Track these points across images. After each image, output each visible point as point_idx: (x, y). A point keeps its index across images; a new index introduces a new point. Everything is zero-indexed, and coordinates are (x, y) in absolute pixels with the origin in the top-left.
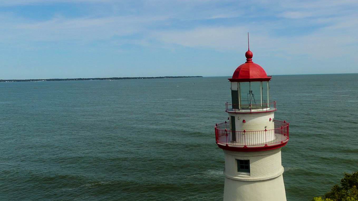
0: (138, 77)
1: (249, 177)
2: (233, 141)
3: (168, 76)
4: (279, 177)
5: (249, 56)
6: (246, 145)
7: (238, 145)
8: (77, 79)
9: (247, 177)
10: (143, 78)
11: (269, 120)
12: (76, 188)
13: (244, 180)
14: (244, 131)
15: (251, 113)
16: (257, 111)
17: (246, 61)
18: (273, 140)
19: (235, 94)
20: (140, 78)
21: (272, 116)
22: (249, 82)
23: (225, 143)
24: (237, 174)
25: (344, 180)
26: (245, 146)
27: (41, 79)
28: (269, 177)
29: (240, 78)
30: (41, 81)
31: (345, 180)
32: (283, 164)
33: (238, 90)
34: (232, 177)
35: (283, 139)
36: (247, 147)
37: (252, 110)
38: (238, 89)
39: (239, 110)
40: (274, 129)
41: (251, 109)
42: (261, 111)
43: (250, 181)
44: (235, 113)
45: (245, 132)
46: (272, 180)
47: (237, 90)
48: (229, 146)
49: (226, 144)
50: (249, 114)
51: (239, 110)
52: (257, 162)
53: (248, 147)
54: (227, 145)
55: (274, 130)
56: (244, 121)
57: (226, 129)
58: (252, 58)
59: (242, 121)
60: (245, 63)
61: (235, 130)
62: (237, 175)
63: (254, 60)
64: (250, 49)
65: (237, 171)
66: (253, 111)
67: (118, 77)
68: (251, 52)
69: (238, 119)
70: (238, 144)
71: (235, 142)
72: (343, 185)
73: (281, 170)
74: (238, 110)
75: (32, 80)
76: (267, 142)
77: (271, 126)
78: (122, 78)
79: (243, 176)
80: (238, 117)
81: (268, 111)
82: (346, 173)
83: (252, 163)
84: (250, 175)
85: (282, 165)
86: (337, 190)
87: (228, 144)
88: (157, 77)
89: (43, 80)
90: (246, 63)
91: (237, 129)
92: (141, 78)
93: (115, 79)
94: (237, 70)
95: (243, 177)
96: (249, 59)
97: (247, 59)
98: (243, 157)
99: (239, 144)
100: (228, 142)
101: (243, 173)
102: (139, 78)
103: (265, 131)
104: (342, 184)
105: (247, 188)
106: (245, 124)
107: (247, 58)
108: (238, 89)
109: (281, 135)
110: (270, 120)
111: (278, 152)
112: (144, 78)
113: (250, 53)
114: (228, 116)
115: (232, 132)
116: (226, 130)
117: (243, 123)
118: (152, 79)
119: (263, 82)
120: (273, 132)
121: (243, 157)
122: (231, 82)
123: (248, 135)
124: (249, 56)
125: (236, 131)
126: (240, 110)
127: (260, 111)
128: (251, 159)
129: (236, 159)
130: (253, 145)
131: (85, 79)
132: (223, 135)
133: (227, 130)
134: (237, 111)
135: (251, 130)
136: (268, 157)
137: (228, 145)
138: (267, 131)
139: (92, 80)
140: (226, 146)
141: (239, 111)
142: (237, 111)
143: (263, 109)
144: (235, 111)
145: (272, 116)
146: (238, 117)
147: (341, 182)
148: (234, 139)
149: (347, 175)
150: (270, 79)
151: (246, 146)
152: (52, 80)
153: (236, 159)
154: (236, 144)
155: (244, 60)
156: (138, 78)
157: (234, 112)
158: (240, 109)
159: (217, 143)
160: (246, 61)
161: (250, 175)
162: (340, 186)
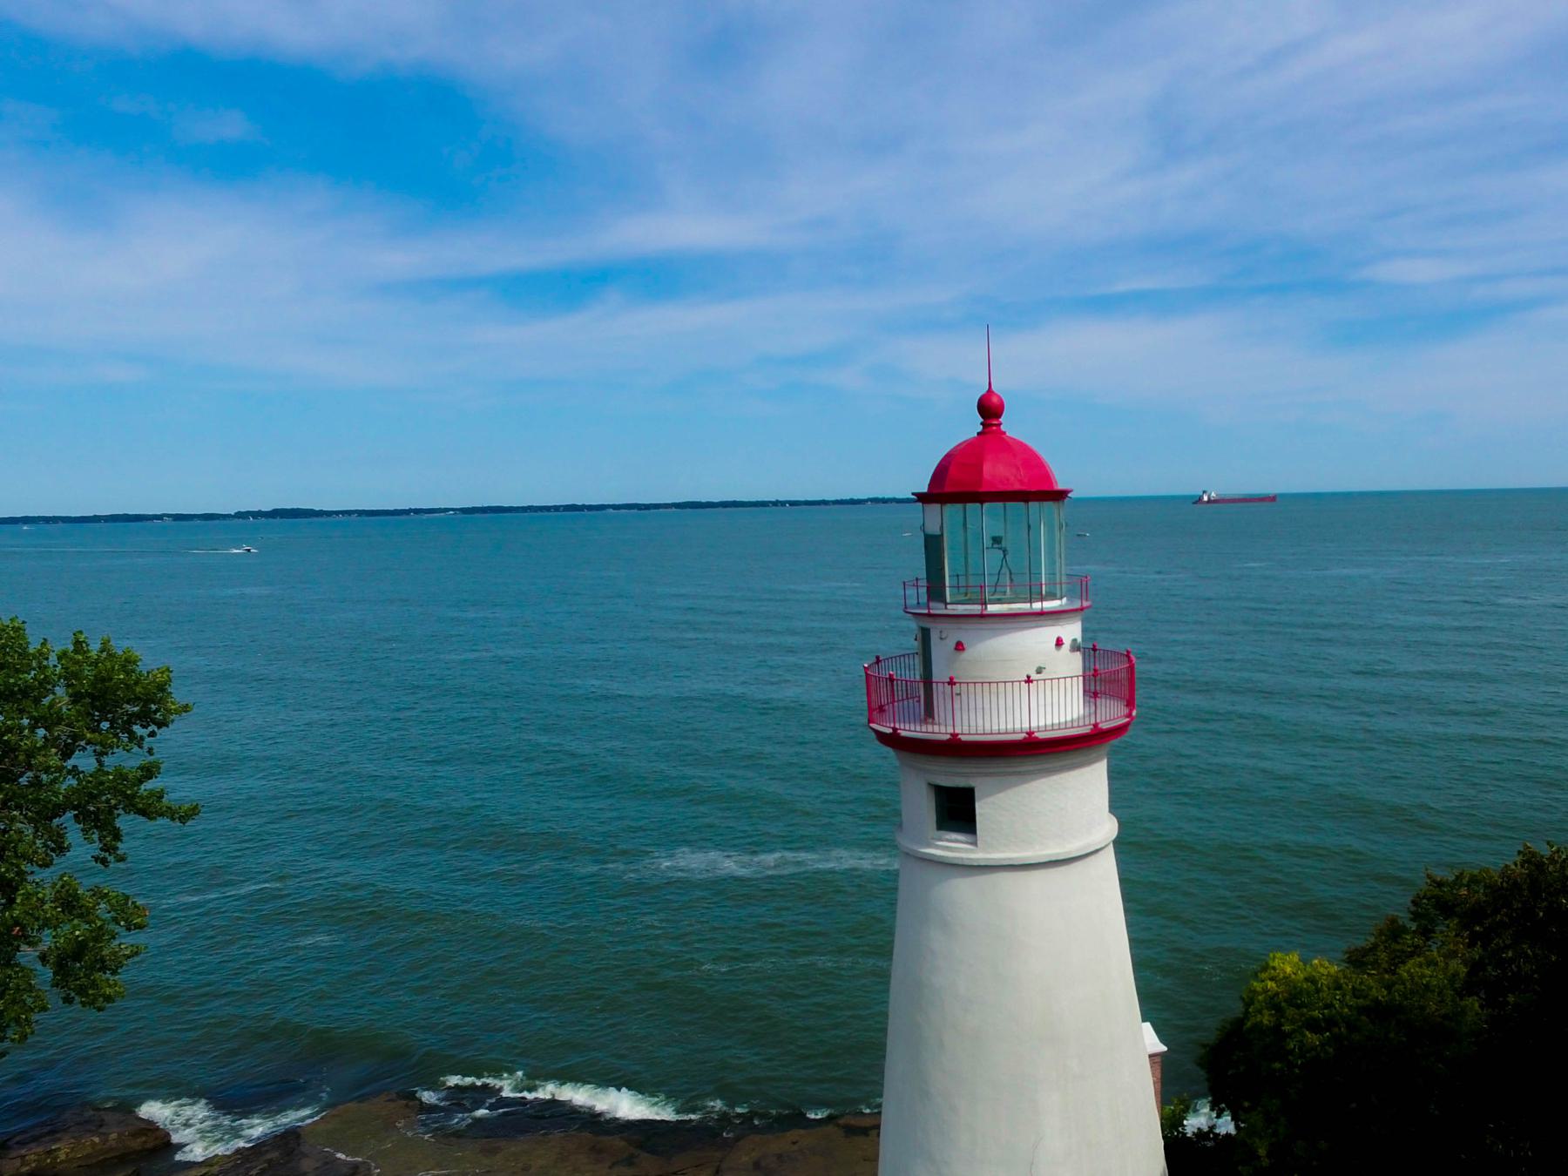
0: (774, 500)
1: (972, 851)
2: (925, 719)
3: (880, 497)
4: (1092, 858)
5: (990, 409)
6: (957, 732)
7: (944, 731)
8: (562, 508)
9: (966, 851)
10: (790, 505)
11: (1055, 643)
12: (786, 1009)
13: (956, 862)
14: (951, 679)
15: (983, 616)
16: (1011, 609)
17: (980, 428)
18: (1075, 716)
19: (933, 546)
20: (780, 502)
21: (1072, 631)
22: (978, 505)
23: (888, 725)
24: (933, 839)
25: (1424, 898)
26: (951, 734)
27: (443, 507)
28: (1044, 852)
29: (948, 489)
30: (442, 514)
31: (1425, 901)
32: (1114, 808)
33: (942, 535)
34: (915, 848)
35: (1111, 713)
36: (960, 739)
37: (989, 606)
38: (942, 528)
39: (946, 604)
40: (1081, 674)
41: (984, 603)
42: (1025, 609)
43: (975, 864)
44: (929, 615)
45: (955, 683)
46: (1063, 865)
47: (939, 533)
48: (903, 733)
49: (892, 725)
50: (974, 620)
51: (946, 604)
52: (1001, 795)
53: (964, 738)
54: (895, 729)
55: (1081, 678)
56: (959, 647)
57: (891, 672)
58: (999, 416)
59: (952, 644)
60: (976, 435)
61: (931, 679)
62: (932, 841)
63: (1011, 425)
64: (993, 387)
65: (935, 825)
66: (992, 608)
67: (703, 501)
68: (999, 397)
69: (941, 639)
70: (936, 728)
71: (930, 720)
72: (1416, 916)
73: (1108, 828)
74: (943, 606)
75: (417, 511)
76: (1032, 725)
77: (1073, 664)
78: (717, 503)
79: (952, 846)
80: (941, 632)
81: (1045, 610)
82: (1429, 872)
83: (983, 801)
84: (975, 843)
85: (1110, 811)
86: (1388, 933)
87: (897, 726)
88: (839, 499)
89: (451, 512)
90: (978, 434)
91: (939, 674)
92: (783, 503)
93: (690, 508)
94: (943, 463)
95: (959, 852)
96: (989, 422)
97: (982, 420)
98: (954, 776)
99: (939, 731)
100: (910, 723)
101: (954, 836)
102: (776, 503)
103: (1026, 682)
104: (1412, 913)
105: (963, 889)
106: (965, 655)
107: (982, 417)
108: (942, 528)
109: (1103, 700)
110: (1059, 643)
111: (1101, 759)
112: (793, 504)
113: (995, 400)
114: (913, 625)
115: (925, 683)
116: (890, 675)
117: (958, 653)
118: (823, 507)
119: (1030, 503)
120: (1077, 688)
121: (954, 776)
122: (923, 503)
123: (972, 697)
124: (990, 409)
125: (934, 680)
126: (949, 607)
127: (1020, 609)
128: (979, 785)
129: (929, 784)
130: (981, 734)
131: (590, 508)
132: (903, 700)
133: (895, 677)
134: (938, 609)
135: (982, 677)
136: (1043, 780)
137: (897, 729)
138: (1032, 681)
139: (611, 510)
140: (890, 734)
141: (946, 608)
142: (938, 609)
143: (1042, 601)
144: (929, 609)
145: (1072, 631)
146: (941, 632)
147: (1410, 904)
148: (929, 713)
149: (1434, 881)
150: (1069, 495)
151: (958, 734)
152: (478, 512)
153: (929, 784)
154: (936, 728)
155: (972, 426)
156: (770, 502)
157: (926, 611)
158: (948, 600)
159: (870, 721)
160: (981, 427)
161: (975, 843)
162: (1404, 917)
